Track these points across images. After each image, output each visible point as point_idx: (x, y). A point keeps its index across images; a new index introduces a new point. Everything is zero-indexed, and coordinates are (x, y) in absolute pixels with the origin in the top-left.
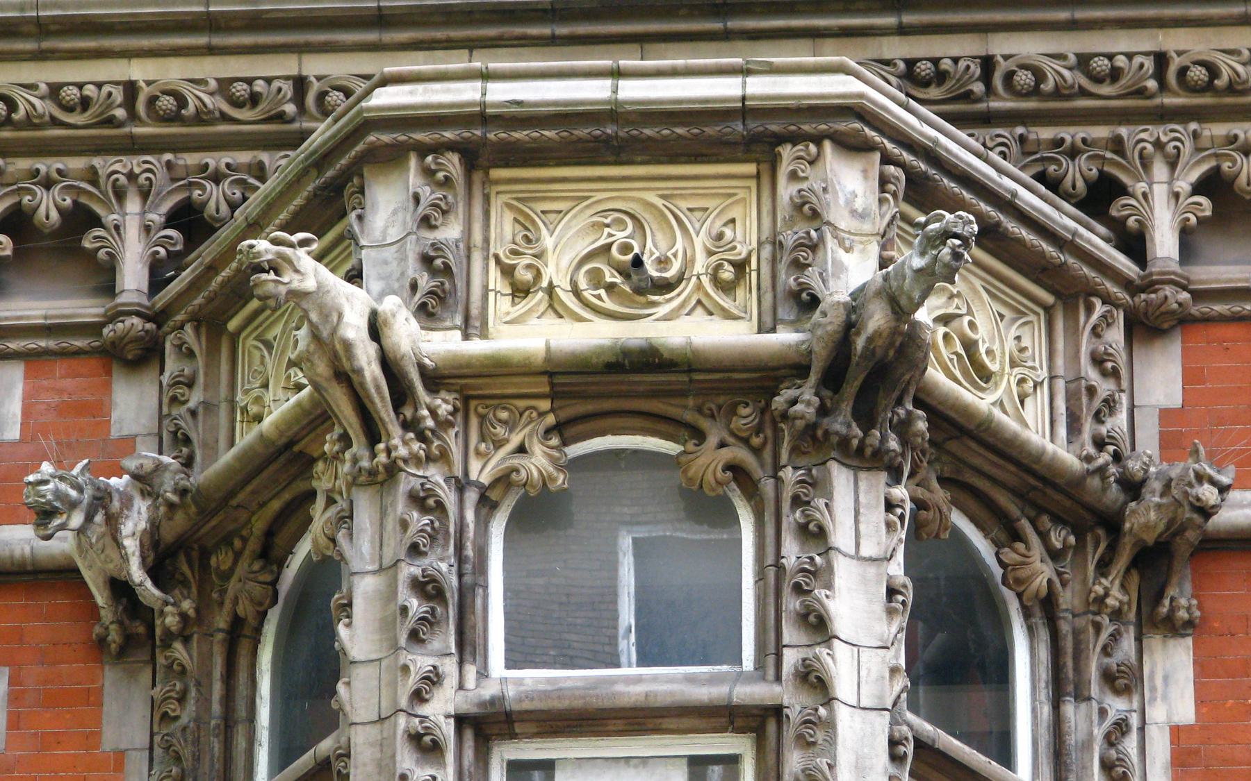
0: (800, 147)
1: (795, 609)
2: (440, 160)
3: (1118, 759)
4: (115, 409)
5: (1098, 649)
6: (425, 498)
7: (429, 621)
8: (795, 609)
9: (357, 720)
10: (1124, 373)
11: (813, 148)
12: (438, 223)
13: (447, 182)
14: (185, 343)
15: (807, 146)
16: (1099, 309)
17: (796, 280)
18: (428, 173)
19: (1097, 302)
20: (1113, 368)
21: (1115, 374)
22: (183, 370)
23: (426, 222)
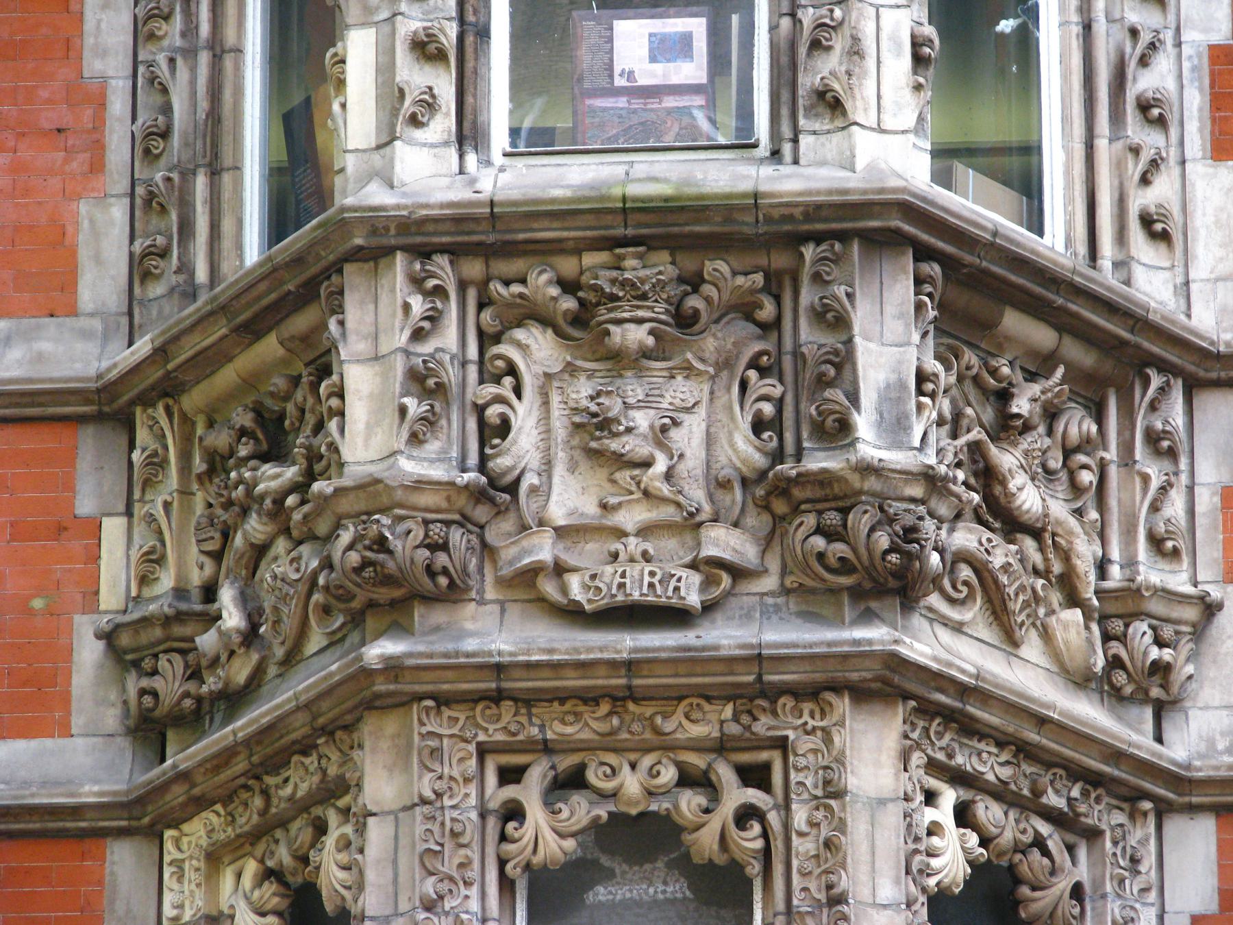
0: (823, 247)
1: (813, 84)
2: (428, 267)
3: (1164, 432)
4: (101, 666)
5: (1144, 405)
6: (426, 377)
7: (429, 421)
8: (813, 84)
9: (349, 147)
10: (1183, 448)
11: (837, 246)
12: (425, 120)
13: (440, 291)
14: (158, 77)
15: (832, 246)
16: (1156, 381)
17: (817, 408)
18: (417, 282)
19: (1152, 372)
20: (1170, 447)
21: (1172, 454)
22: (156, 120)
23: (418, 335)
